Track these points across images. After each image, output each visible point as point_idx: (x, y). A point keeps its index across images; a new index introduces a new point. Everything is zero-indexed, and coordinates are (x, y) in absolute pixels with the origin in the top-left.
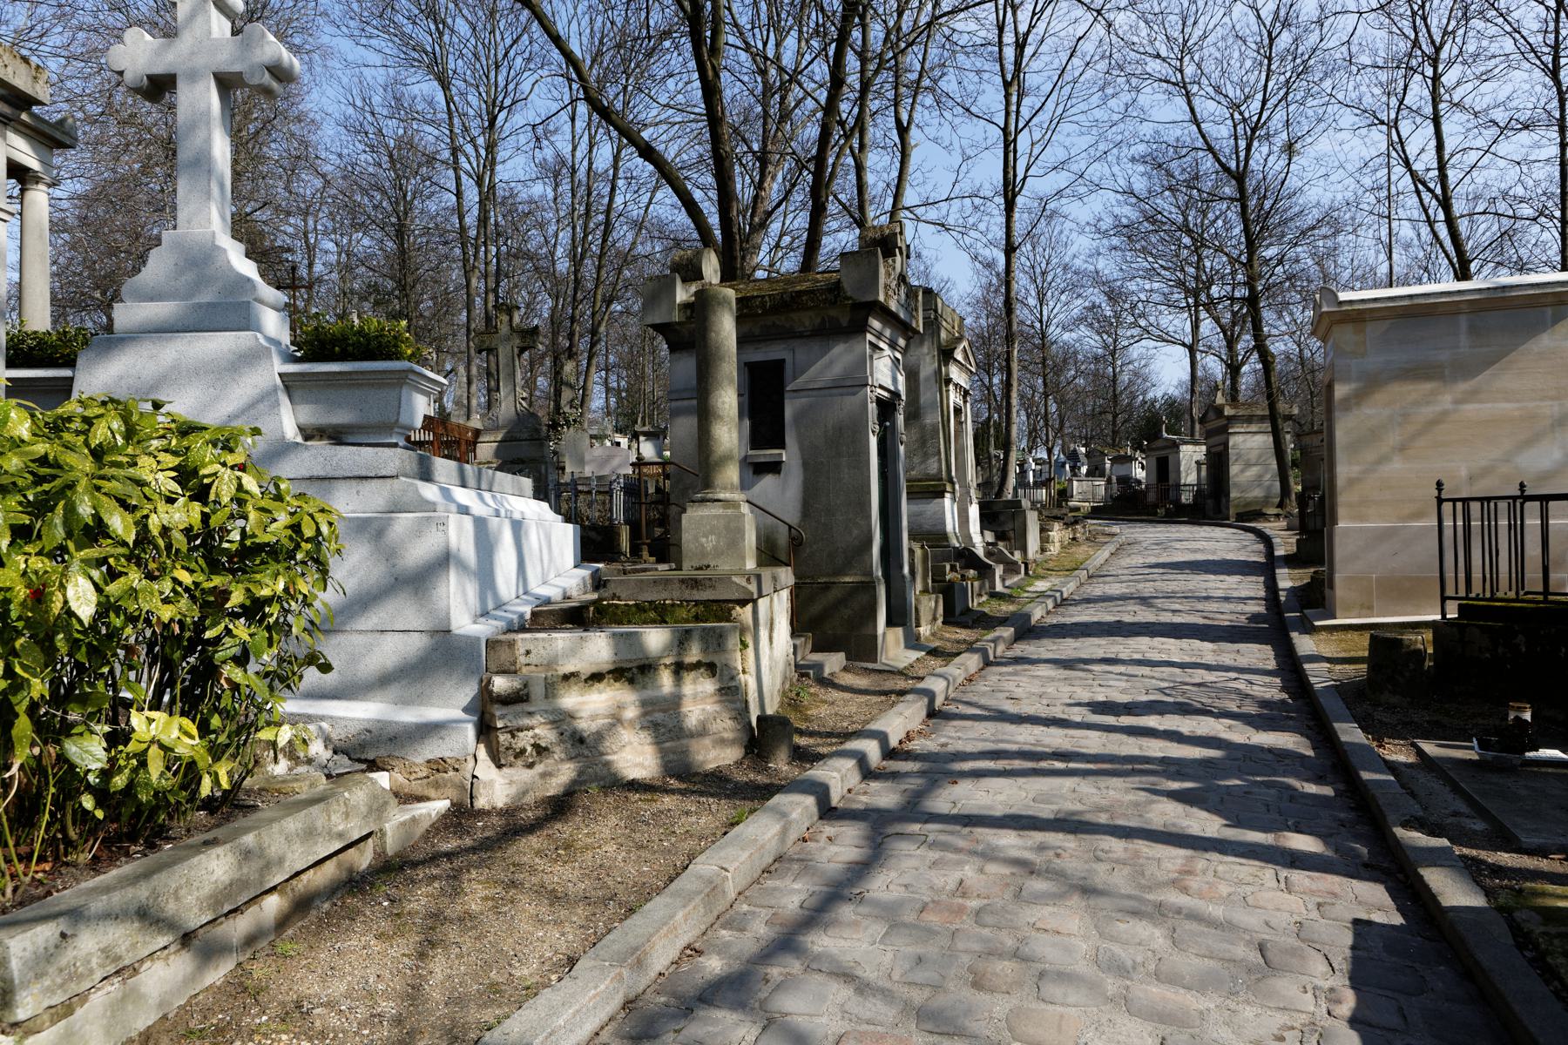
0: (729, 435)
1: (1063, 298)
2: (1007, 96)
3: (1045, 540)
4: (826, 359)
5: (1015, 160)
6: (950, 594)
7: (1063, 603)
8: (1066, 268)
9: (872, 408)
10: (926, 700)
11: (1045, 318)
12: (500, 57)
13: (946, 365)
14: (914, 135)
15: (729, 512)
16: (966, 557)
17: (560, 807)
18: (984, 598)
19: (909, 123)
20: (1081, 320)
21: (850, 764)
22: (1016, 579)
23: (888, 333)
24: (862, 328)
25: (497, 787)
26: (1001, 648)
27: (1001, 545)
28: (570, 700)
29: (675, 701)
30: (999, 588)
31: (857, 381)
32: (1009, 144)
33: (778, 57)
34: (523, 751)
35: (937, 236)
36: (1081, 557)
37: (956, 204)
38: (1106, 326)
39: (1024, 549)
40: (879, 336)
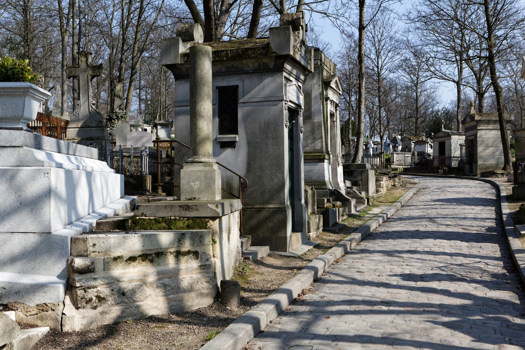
0: (207, 126)
1: (390, 54)
3: (378, 186)
4: (261, 85)
6: (326, 215)
7: (388, 220)
8: (391, 38)
9: (286, 113)
10: (313, 272)
11: (380, 66)
13: (326, 90)
15: (207, 168)
16: (336, 195)
18: (345, 217)
20: (400, 66)
21: (271, 307)
23: (295, 72)
24: (280, 69)
26: (354, 244)
27: (355, 189)
28: (117, 271)
29: (176, 272)
30: (353, 211)
31: (277, 98)
35: (322, 19)
36: (397, 195)
38: (412, 70)
40: (290, 73)
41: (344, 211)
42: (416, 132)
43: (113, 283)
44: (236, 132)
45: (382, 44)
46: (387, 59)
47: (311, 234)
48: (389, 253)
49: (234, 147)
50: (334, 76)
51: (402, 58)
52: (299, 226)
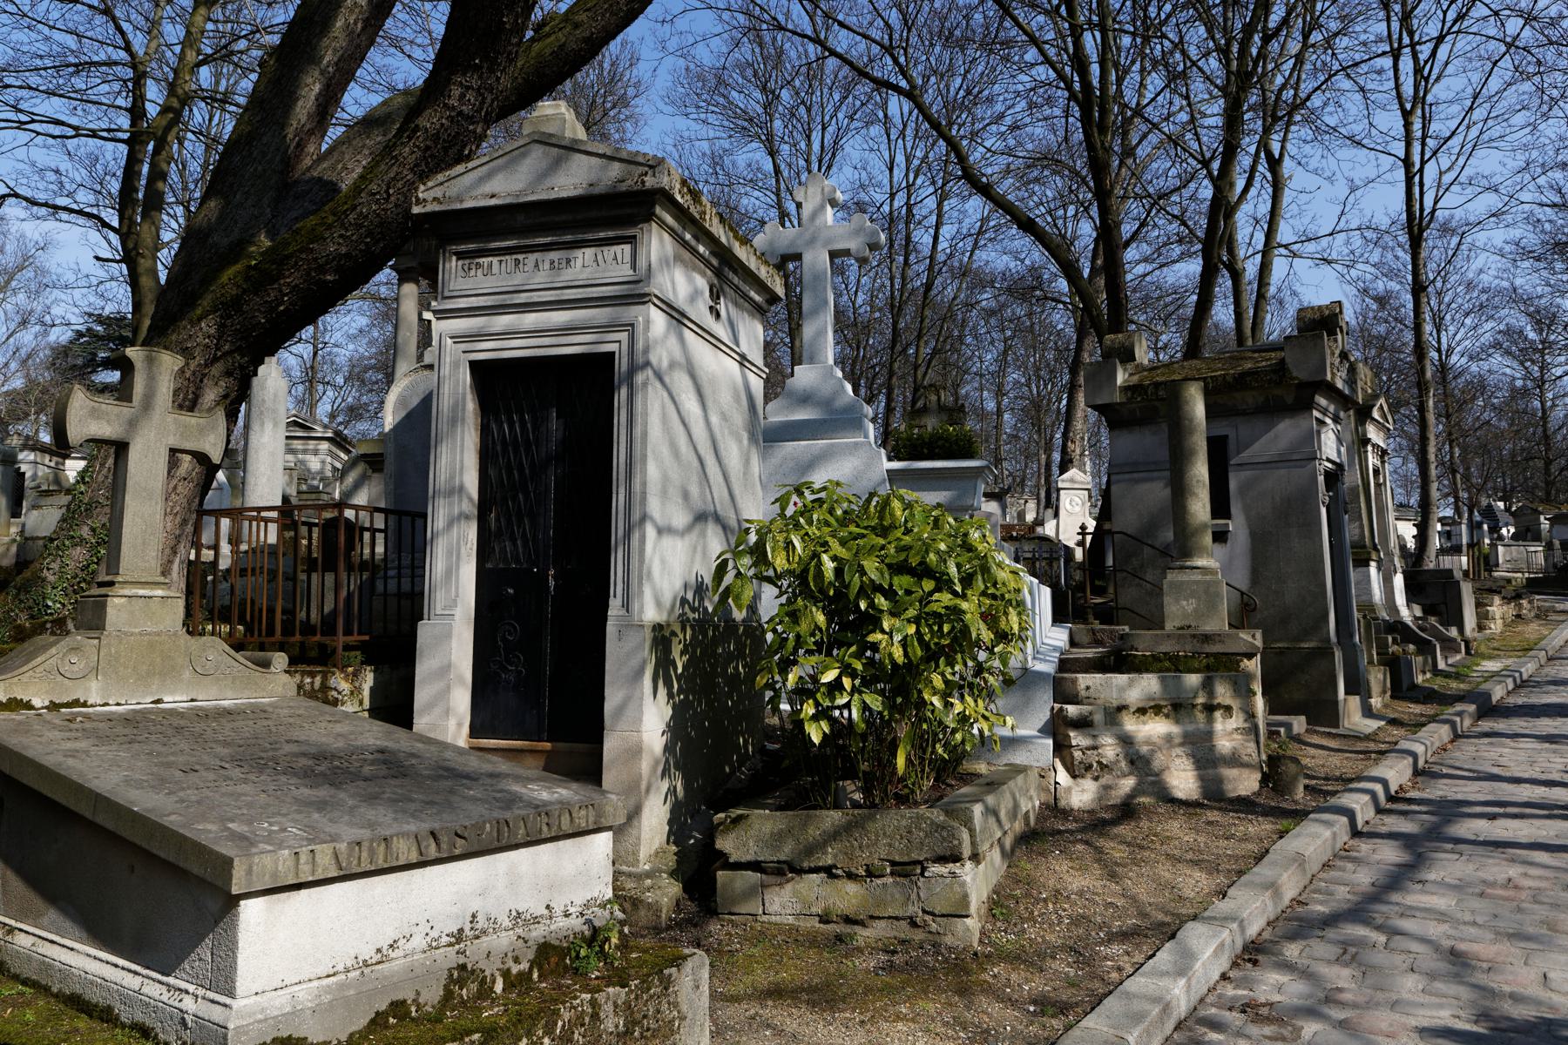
0: (1200, 507)
1: (1468, 321)
2: (1408, 125)
3: (1483, 618)
4: (1271, 434)
5: (1422, 194)
6: (1397, 670)
7: (1522, 685)
8: (1470, 286)
9: (1321, 479)
10: (1411, 759)
11: (1444, 346)
12: (827, 118)
13: (1363, 424)
14: (1288, 166)
15: (1208, 578)
16: (1397, 627)
17: (1127, 811)
18: (1428, 675)
19: (1281, 155)
20: (1497, 345)
21: (1367, 798)
22: (1458, 657)
23: (1332, 408)
24: (1309, 405)
25: (1081, 795)
26: (1467, 722)
27: (1433, 620)
28: (1130, 725)
29: (1209, 734)
30: (1441, 665)
31: (1307, 452)
32: (1412, 176)
33: (1119, 91)
34: (1091, 766)
35: (1315, 270)
36: (1533, 637)
37: (1341, 237)
38: (1526, 353)
39: (1461, 630)
40: (1324, 412)
41: (1425, 662)
42: (1548, 494)
43: (1126, 741)
44: (1228, 516)
45: (1446, 299)
46: (1462, 330)
47: (1373, 701)
48: (1551, 739)
49: (1225, 541)
50: (1376, 397)
51: (1502, 327)
52: (1357, 686)
